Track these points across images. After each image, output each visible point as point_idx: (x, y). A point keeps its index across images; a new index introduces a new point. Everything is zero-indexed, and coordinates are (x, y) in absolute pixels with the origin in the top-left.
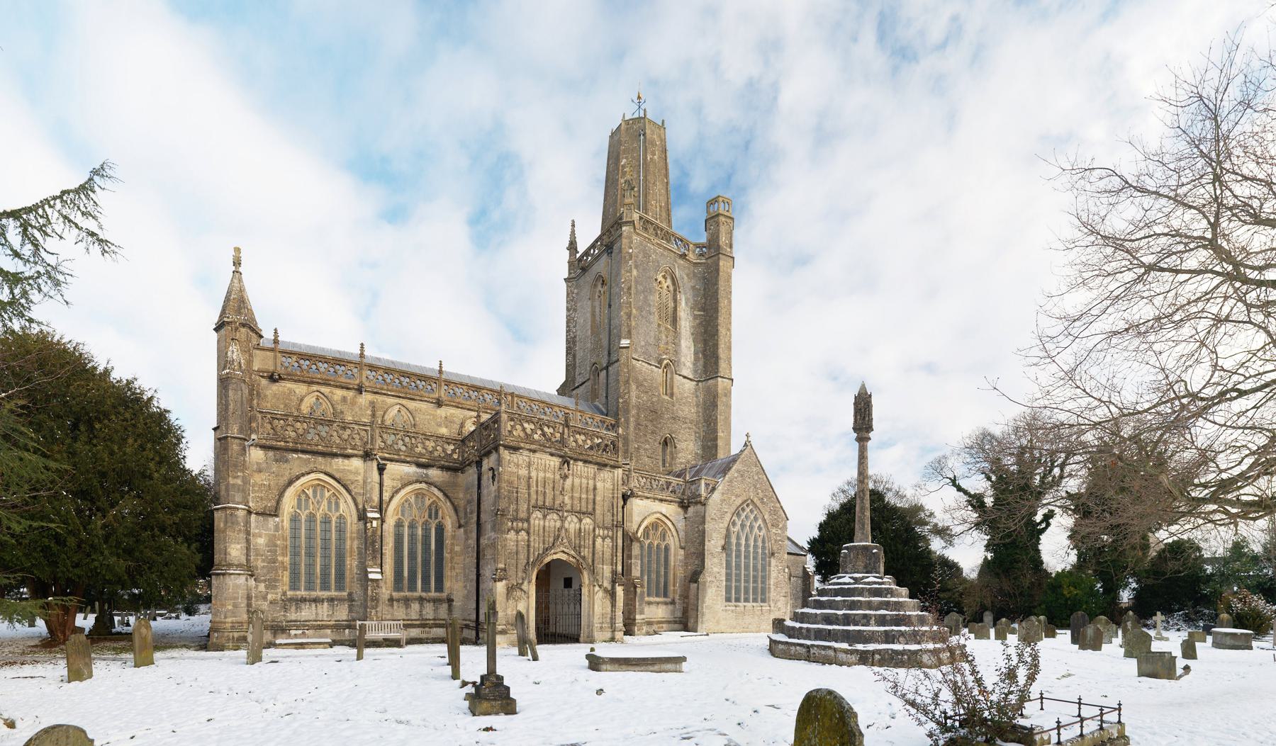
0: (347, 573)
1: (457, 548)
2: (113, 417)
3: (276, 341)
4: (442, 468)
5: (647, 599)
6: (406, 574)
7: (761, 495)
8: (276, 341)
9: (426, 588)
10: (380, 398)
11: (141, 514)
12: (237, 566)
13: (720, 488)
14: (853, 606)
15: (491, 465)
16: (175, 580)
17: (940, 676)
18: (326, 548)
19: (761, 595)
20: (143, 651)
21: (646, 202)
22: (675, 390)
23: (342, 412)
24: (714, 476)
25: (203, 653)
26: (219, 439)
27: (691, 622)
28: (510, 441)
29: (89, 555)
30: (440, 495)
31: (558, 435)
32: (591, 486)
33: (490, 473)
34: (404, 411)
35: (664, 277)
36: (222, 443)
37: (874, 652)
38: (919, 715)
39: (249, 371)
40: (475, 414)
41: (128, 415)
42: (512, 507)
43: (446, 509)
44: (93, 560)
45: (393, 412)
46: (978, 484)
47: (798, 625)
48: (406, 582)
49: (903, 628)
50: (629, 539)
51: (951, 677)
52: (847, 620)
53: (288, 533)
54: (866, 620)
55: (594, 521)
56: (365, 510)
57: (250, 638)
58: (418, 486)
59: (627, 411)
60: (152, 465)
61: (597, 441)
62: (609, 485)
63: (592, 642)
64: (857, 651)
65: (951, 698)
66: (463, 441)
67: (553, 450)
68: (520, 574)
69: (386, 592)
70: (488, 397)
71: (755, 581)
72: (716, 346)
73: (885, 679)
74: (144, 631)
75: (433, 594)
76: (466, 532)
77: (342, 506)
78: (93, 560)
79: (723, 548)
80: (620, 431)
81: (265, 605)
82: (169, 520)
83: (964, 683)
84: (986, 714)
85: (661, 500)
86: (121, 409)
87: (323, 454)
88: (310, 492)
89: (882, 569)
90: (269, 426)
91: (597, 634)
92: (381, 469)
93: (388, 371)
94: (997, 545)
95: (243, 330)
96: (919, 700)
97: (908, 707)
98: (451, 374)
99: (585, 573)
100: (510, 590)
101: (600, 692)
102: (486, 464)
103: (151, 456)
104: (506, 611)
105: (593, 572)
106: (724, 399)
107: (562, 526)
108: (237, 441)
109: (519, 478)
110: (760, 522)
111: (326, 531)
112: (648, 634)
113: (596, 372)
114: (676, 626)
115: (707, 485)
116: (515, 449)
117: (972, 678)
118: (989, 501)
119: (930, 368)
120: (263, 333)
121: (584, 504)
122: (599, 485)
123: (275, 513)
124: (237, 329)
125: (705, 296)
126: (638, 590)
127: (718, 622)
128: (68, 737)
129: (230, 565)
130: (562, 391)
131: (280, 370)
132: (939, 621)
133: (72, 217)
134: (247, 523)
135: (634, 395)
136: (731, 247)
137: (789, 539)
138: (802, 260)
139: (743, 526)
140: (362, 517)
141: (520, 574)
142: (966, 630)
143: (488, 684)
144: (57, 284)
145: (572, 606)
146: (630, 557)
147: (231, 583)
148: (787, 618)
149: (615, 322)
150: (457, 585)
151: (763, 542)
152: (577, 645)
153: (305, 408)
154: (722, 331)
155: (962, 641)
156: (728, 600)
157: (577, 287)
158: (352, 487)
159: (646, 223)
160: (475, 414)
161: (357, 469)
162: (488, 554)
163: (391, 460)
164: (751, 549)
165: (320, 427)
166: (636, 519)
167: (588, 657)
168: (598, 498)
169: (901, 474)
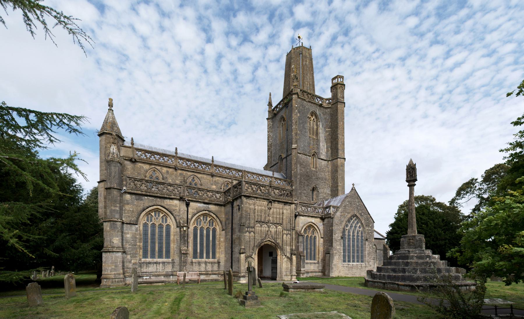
3: (132, 144)
6: (199, 251)
7: (360, 212)
9: (208, 257)
22: (318, 166)
23: (166, 178)
33: (238, 207)
48: (198, 254)
50: (299, 235)
55: (283, 227)
59: (296, 177)
62: (289, 212)
68: (251, 251)
71: (358, 252)
72: (337, 144)
75: (211, 260)
76: (226, 232)
79: (342, 238)
85: (312, 217)
89: (424, 246)
93: (188, 160)
102: (235, 204)
105: (282, 249)
107: (269, 230)
109: (250, 209)
110: (359, 224)
111: (161, 232)
120: (125, 139)
121: (278, 220)
122: (285, 211)
126: (302, 257)
136: (343, 98)
139: (351, 227)
141: (251, 251)
151: (362, 233)
154: (340, 136)
156: (344, 261)
158: (173, 212)
159: (303, 92)
162: (237, 242)
163: (192, 201)
164: (356, 237)
168: (284, 217)
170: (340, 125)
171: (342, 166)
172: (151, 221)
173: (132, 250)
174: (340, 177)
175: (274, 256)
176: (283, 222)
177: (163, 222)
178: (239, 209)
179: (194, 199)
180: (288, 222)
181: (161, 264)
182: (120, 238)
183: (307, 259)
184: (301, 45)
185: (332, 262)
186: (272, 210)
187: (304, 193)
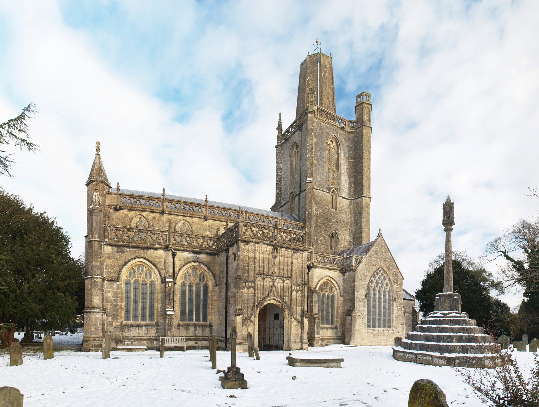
0: (155, 311)
1: (215, 298)
2: (34, 232)
3: (118, 189)
4: (207, 254)
5: (321, 326)
6: (187, 311)
7: (388, 265)
8: (118, 189)
9: (198, 319)
10: (173, 217)
11: (47, 282)
12: (97, 308)
13: (364, 261)
14: (442, 330)
15: (234, 251)
16: (65, 315)
17: (495, 373)
18: (144, 298)
19: (388, 324)
20: (49, 351)
21: (321, 100)
23: (153, 225)
24: (360, 255)
25: (79, 353)
26: (88, 242)
27: (346, 340)
28: (244, 238)
29: (21, 303)
30: (206, 268)
31: (271, 234)
32: (290, 262)
34: (186, 223)
35: (331, 141)
36: (89, 244)
37: (455, 358)
38: (483, 397)
39: (104, 205)
40: (225, 223)
41: (41, 231)
42: (246, 274)
43: (209, 276)
44: (23, 305)
45: (180, 224)
46: (520, 255)
47: (410, 341)
48: (187, 316)
49: (473, 344)
50: (311, 291)
51: (502, 374)
52: (439, 339)
53: (124, 290)
54: (450, 339)
55: (291, 282)
56: (165, 278)
57: (104, 346)
58: (193, 264)
59: (310, 219)
60: (53, 256)
61: (293, 236)
62: (300, 261)
63: (290, 350)
64: (445, 357)
65: (503, 387)
66: (218, 239)
67: (268, 242)
68: (250, 312)
69: (176, 321)
70: (232, 214)
71: (384, 316)
72: (362, 179)
73: (462, 374)
74: (49, 341)
75: (202, 322)
76: (220, 289)
77: (153, 275)
78: (23, 305)
79: (366, 296)
80: (307, 230)
81: (111, 328)
82: (62, 284)
83: (511, 378)
84: (524, 397)
85: (330, 269)
86: (38, 228)
87: (143, 248)
88: (136, 269)
89: (460, 308)
90: (114, 234)
91: (293, 346)
92: (174, 255)
93: (178, 202)
94: (531, 293)
95: (101, 184)
96: (483, 387)
97: (476, 391)
98: (212, 202)
99: (286, 312)
100: (244, 321)
101: (294, 378)
102: (231, 251)
103: (53, 251)
104: (241, 332)
105: (291, 310)
106: (366, 209)
107: (273, 285)
108: (97, 242)
109: (249, 258)
110: (387, 281)
111: (144, 289)
112: (322, 345)
113: (293, 197)
114: (338, 341)
115: (356, 260)
116: (247, 242)
117: (515, 375)
118: (526, 266)
119: (489, 185)
120: (111, 186)
121: (285, 272)
123: (117, 279)
124: (97, 184)
125: (355, 150)
126: (317, 321)
127: (363, 339)
128: (10, 393)
129: (93, 308)
130: (274, 209)
131: (120, 204)
132: (495, 340)
133: (13, 133)
134: (103, 285)
135: (314, 209)
136: (370, 121)
137: (404, 290)
138: (412, 125)
139: (377, 283)
140: (164, 281)
141: (250, 312)
142: (512, 346)
143: (231, 372)
144: (6, 166)
145: (279, 330)
146: (312, 302)
147: (94, 317)
148: (403, 337)
149: (304, 168)
150: (215, 318)
151: (389, 292)
152: (282, 352)
153: (133, 224)
154: (365, 169)
155: (509, 352)
156: (369, 326)
157: (282, 150)
158: (158, 265)
159: (321, 111)
160: (225, 223)
161: (161, 256)
162: (232, 300)
163: (179, 250)
164: (382, 297)
165: (141, 234)
166: (316, 280)
167: (288, 358)
168: (294, 269)
169: (471, 250)
170: (365, 155)
171: (367, 207)
172: (134, 277)
173: (113, 311)
174: (364, 220)
175: (280, 318)
176: (291, 275)
177: (146, 277)
178: (235, 259)
179: (182, 248)
180: (298, 274)
181: (144, 328)
182: (101, 297)
183: (322, 324)
184: (319, 51)
185: (354, 327)
186: (277, 260)
187: (321, 240)
